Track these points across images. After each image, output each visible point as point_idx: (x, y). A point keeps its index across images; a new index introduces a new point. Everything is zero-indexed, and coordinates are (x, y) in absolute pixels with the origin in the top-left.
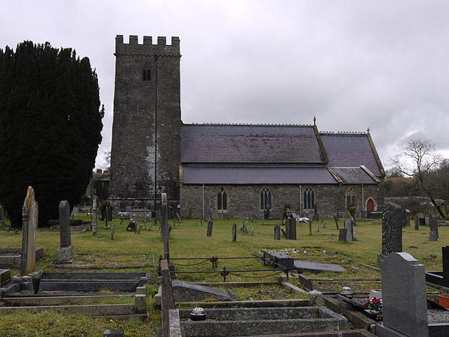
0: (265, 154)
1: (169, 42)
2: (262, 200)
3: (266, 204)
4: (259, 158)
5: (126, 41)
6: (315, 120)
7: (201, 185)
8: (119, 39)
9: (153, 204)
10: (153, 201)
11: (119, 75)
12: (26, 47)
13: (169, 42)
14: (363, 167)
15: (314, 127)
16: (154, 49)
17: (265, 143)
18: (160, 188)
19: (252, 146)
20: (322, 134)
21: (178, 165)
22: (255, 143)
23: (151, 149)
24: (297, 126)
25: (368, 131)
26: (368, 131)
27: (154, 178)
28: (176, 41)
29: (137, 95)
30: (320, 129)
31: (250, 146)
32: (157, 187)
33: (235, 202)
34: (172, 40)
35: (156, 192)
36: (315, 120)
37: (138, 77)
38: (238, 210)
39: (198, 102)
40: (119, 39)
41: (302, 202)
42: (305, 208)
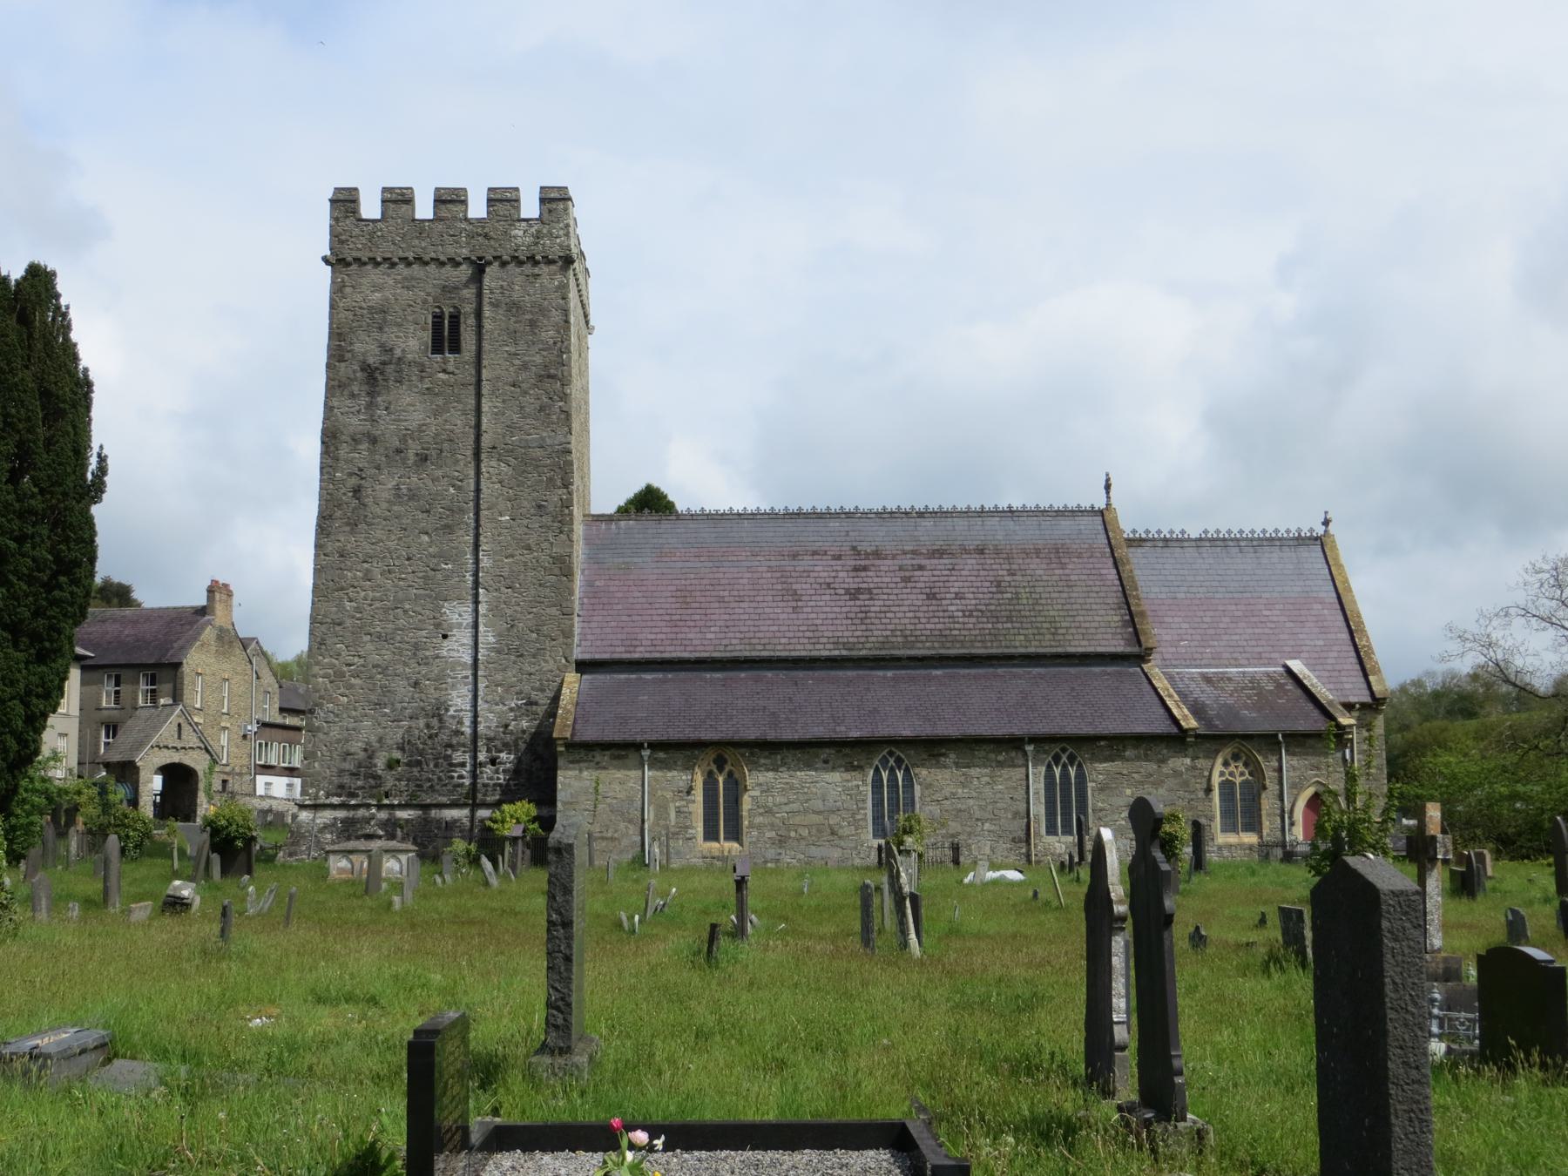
0: (901, 617)
1: (530, 208)
2: (878, 803)
3: (894, 808)
4: (878, 633)
5: (370, 208)
6: (1108, 487)
7: (638, 746)
8: (344, 202)
9: (466, 821)
10: (466, 812)
11: (342, 242)
12: (83, 388)
13: (530, 208)
14: (1296, 666)
15: (1104, 516)
16: (471, 236)
17: (907, 580)
18: (493, 762)
19: (854, 594)
20: (1136, 542)
21: (563, 670)
22: (870, 579)
23: (458, 614)
24: (1039, 513)
25: (1326, 523)
26: (1326, 523)
27: (467, 722)
28: (555, 200)
29: (409, 408)
30: (1129, 522)
31: (847, 591)
32: (482, 757)
33: (769, 811)
34: (542, 201)
35: (474, 776)
36: (1108, 487)
37: (413, 342)
38: (782, 841)
39: (681, 408)
40: (344, 202)
41: (1038, 809)
42: (1051, 830)
